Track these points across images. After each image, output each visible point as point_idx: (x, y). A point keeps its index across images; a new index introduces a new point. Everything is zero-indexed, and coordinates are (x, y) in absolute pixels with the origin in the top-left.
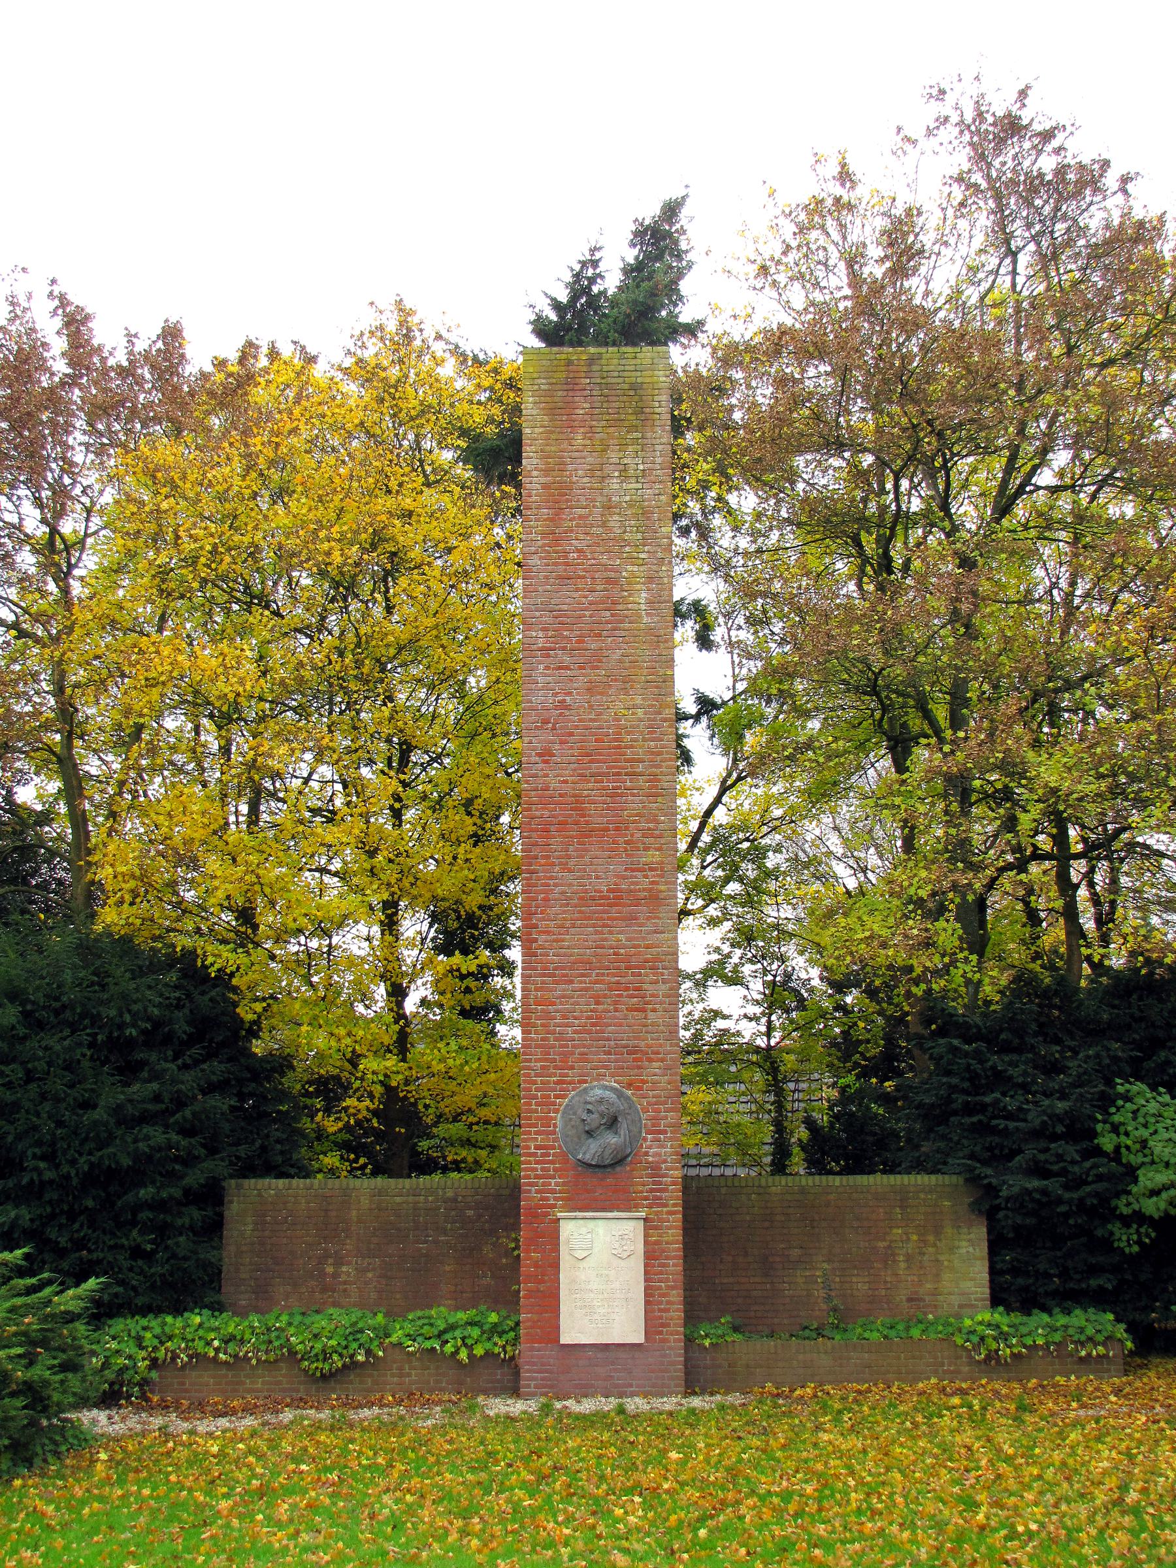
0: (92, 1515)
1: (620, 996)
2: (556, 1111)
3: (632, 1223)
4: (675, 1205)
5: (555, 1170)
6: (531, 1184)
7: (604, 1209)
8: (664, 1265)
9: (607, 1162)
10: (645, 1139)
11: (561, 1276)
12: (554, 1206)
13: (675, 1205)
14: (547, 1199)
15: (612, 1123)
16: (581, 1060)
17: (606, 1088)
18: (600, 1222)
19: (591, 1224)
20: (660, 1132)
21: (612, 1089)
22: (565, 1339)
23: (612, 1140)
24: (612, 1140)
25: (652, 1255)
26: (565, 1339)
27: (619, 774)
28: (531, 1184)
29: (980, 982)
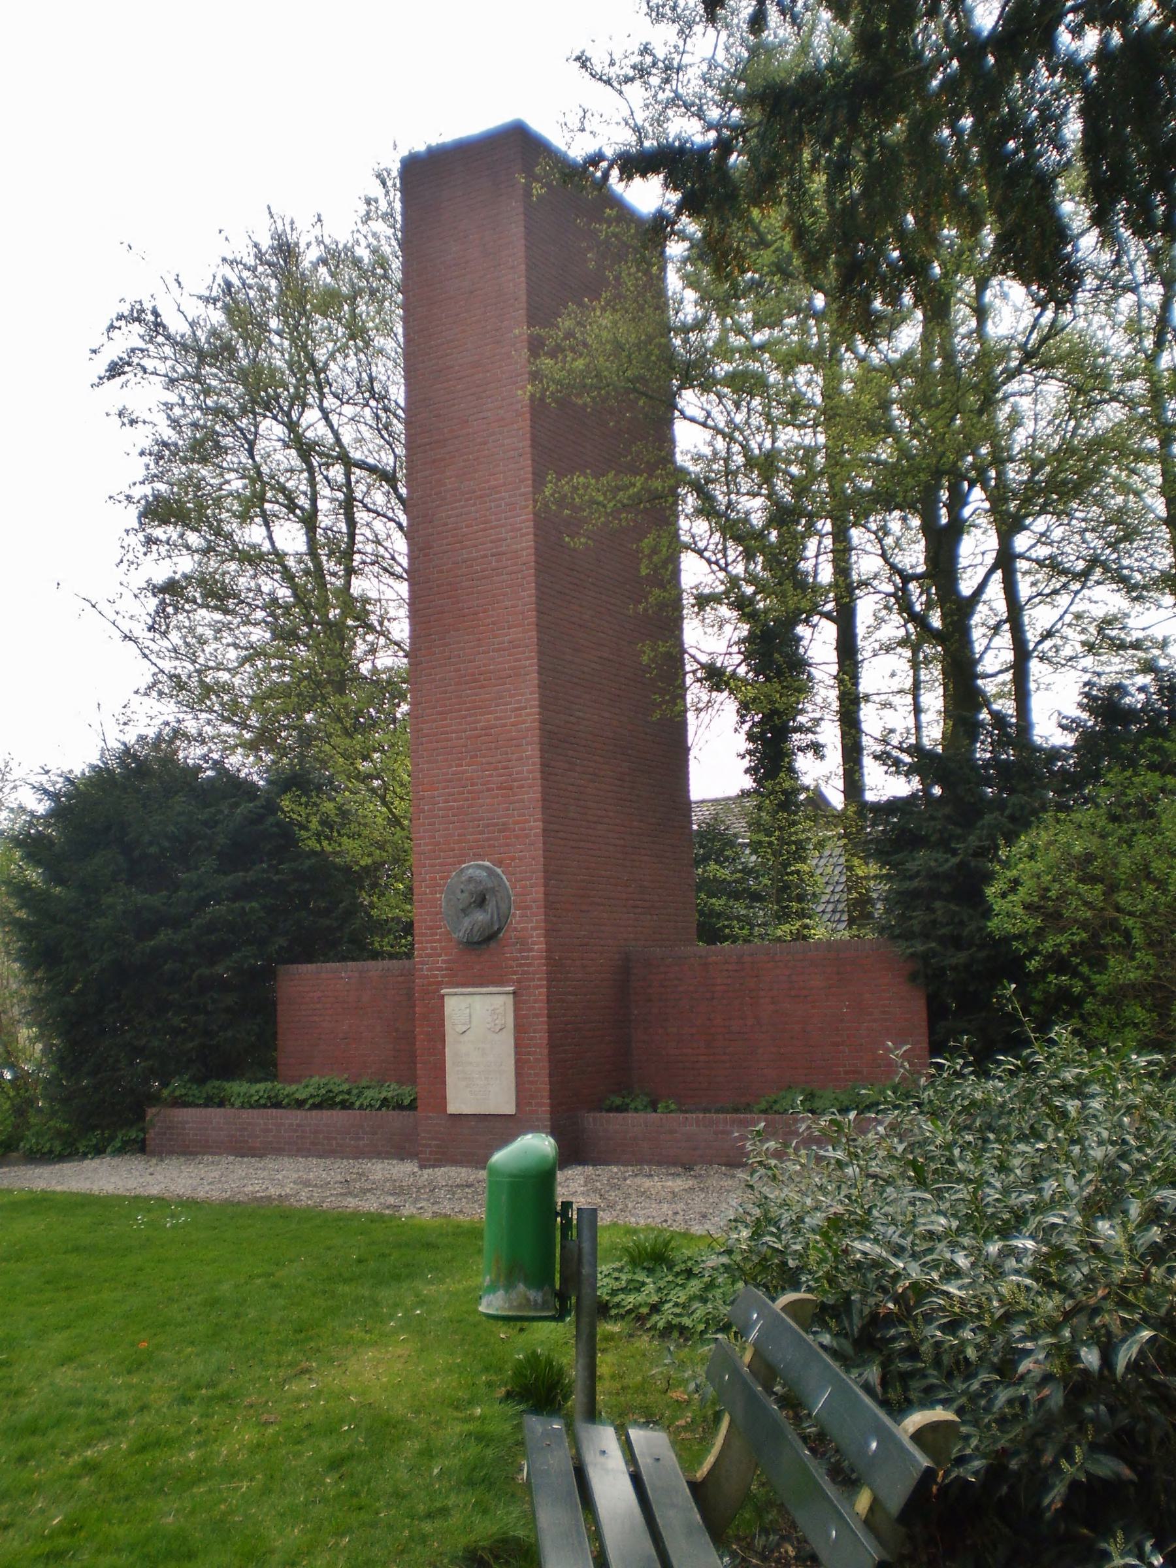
0: (173, 1227)
1: (491, 776)
2: (441, 893)
3: (502, 998)
4: (540, 979)
5: (443, 948)
6: (423, 963)
7: (481, 985)
8: (531, 1039)
9: (475, 940)
10: (514, 914)
11: (447, 1050)
12: (440, 983)
13: (540, 979)
14: (436, 976)
15: (481, 901)
16: (459, 842)
17: (479, 867)
18: (477, 998)
19: (469, 999)
20: (527, 907)
21: (487, 868)
22: (452, 1109)
23: (480, 917)
24: (480, 917)
25: (521, 1030)
26: (452, 1109)
27: (485, 556)
28: (423, 963)
29: (914, 1158)
